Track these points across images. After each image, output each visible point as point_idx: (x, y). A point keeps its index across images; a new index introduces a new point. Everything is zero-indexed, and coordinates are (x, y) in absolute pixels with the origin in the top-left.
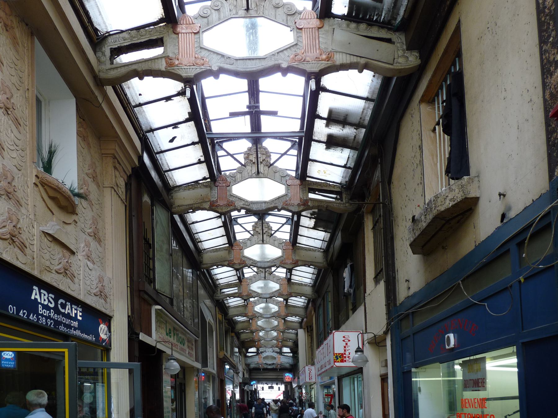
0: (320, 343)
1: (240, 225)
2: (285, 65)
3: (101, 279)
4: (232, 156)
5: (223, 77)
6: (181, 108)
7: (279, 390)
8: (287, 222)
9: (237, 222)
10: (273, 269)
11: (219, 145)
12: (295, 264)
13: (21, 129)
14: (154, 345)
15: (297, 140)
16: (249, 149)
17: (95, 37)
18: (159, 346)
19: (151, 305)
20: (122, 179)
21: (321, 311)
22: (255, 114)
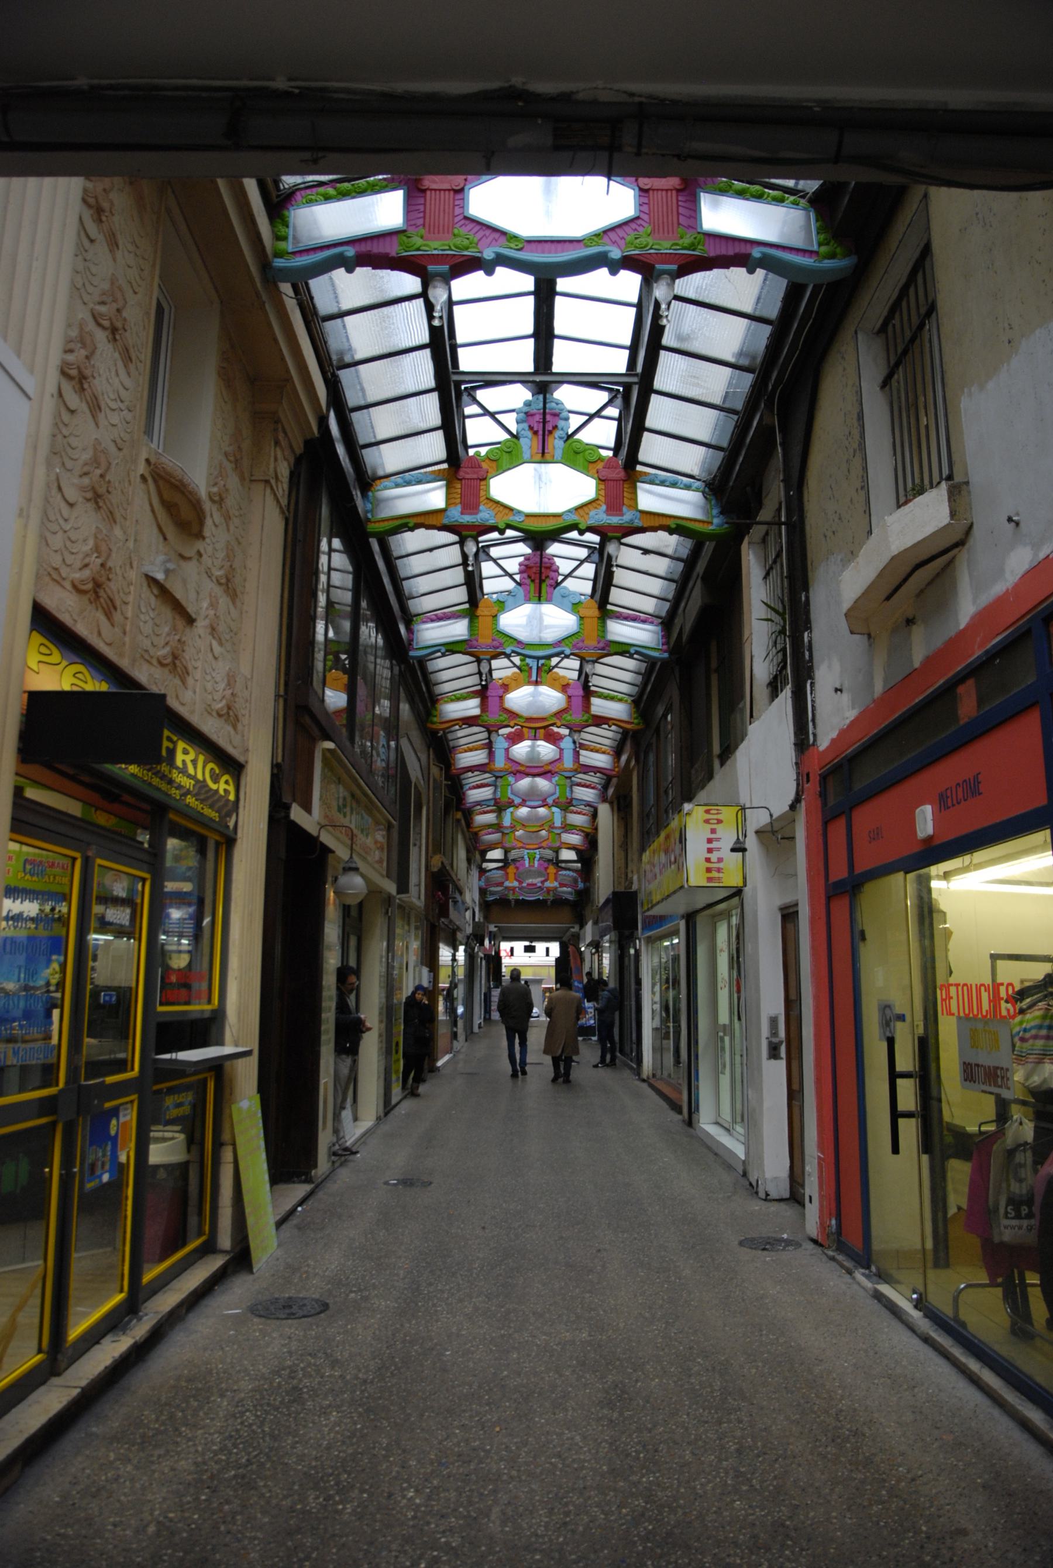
0: (647, 838)
1: (495, 561)
2: (616, 254)
3: (231, 680)
4: (492, 415)
5: (500, 271)
6: (411, 325)
7: (547, 955)
8: (589, 556)
9: (488, 554)
10: (555, 660)
11: (470, 395)
12: (603, 649)
13: (132, 367)
14: (315, 833)
15: (621, 389)
16: (527, 404)
17: (274, 194)
18: (326, 839)
19: (313, 741)
20: (285, 464)
21: (652, 758)
22: (544, 334)
